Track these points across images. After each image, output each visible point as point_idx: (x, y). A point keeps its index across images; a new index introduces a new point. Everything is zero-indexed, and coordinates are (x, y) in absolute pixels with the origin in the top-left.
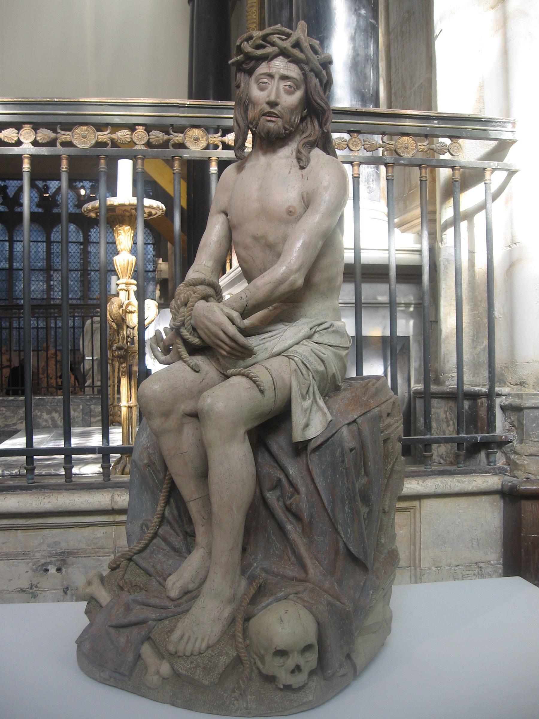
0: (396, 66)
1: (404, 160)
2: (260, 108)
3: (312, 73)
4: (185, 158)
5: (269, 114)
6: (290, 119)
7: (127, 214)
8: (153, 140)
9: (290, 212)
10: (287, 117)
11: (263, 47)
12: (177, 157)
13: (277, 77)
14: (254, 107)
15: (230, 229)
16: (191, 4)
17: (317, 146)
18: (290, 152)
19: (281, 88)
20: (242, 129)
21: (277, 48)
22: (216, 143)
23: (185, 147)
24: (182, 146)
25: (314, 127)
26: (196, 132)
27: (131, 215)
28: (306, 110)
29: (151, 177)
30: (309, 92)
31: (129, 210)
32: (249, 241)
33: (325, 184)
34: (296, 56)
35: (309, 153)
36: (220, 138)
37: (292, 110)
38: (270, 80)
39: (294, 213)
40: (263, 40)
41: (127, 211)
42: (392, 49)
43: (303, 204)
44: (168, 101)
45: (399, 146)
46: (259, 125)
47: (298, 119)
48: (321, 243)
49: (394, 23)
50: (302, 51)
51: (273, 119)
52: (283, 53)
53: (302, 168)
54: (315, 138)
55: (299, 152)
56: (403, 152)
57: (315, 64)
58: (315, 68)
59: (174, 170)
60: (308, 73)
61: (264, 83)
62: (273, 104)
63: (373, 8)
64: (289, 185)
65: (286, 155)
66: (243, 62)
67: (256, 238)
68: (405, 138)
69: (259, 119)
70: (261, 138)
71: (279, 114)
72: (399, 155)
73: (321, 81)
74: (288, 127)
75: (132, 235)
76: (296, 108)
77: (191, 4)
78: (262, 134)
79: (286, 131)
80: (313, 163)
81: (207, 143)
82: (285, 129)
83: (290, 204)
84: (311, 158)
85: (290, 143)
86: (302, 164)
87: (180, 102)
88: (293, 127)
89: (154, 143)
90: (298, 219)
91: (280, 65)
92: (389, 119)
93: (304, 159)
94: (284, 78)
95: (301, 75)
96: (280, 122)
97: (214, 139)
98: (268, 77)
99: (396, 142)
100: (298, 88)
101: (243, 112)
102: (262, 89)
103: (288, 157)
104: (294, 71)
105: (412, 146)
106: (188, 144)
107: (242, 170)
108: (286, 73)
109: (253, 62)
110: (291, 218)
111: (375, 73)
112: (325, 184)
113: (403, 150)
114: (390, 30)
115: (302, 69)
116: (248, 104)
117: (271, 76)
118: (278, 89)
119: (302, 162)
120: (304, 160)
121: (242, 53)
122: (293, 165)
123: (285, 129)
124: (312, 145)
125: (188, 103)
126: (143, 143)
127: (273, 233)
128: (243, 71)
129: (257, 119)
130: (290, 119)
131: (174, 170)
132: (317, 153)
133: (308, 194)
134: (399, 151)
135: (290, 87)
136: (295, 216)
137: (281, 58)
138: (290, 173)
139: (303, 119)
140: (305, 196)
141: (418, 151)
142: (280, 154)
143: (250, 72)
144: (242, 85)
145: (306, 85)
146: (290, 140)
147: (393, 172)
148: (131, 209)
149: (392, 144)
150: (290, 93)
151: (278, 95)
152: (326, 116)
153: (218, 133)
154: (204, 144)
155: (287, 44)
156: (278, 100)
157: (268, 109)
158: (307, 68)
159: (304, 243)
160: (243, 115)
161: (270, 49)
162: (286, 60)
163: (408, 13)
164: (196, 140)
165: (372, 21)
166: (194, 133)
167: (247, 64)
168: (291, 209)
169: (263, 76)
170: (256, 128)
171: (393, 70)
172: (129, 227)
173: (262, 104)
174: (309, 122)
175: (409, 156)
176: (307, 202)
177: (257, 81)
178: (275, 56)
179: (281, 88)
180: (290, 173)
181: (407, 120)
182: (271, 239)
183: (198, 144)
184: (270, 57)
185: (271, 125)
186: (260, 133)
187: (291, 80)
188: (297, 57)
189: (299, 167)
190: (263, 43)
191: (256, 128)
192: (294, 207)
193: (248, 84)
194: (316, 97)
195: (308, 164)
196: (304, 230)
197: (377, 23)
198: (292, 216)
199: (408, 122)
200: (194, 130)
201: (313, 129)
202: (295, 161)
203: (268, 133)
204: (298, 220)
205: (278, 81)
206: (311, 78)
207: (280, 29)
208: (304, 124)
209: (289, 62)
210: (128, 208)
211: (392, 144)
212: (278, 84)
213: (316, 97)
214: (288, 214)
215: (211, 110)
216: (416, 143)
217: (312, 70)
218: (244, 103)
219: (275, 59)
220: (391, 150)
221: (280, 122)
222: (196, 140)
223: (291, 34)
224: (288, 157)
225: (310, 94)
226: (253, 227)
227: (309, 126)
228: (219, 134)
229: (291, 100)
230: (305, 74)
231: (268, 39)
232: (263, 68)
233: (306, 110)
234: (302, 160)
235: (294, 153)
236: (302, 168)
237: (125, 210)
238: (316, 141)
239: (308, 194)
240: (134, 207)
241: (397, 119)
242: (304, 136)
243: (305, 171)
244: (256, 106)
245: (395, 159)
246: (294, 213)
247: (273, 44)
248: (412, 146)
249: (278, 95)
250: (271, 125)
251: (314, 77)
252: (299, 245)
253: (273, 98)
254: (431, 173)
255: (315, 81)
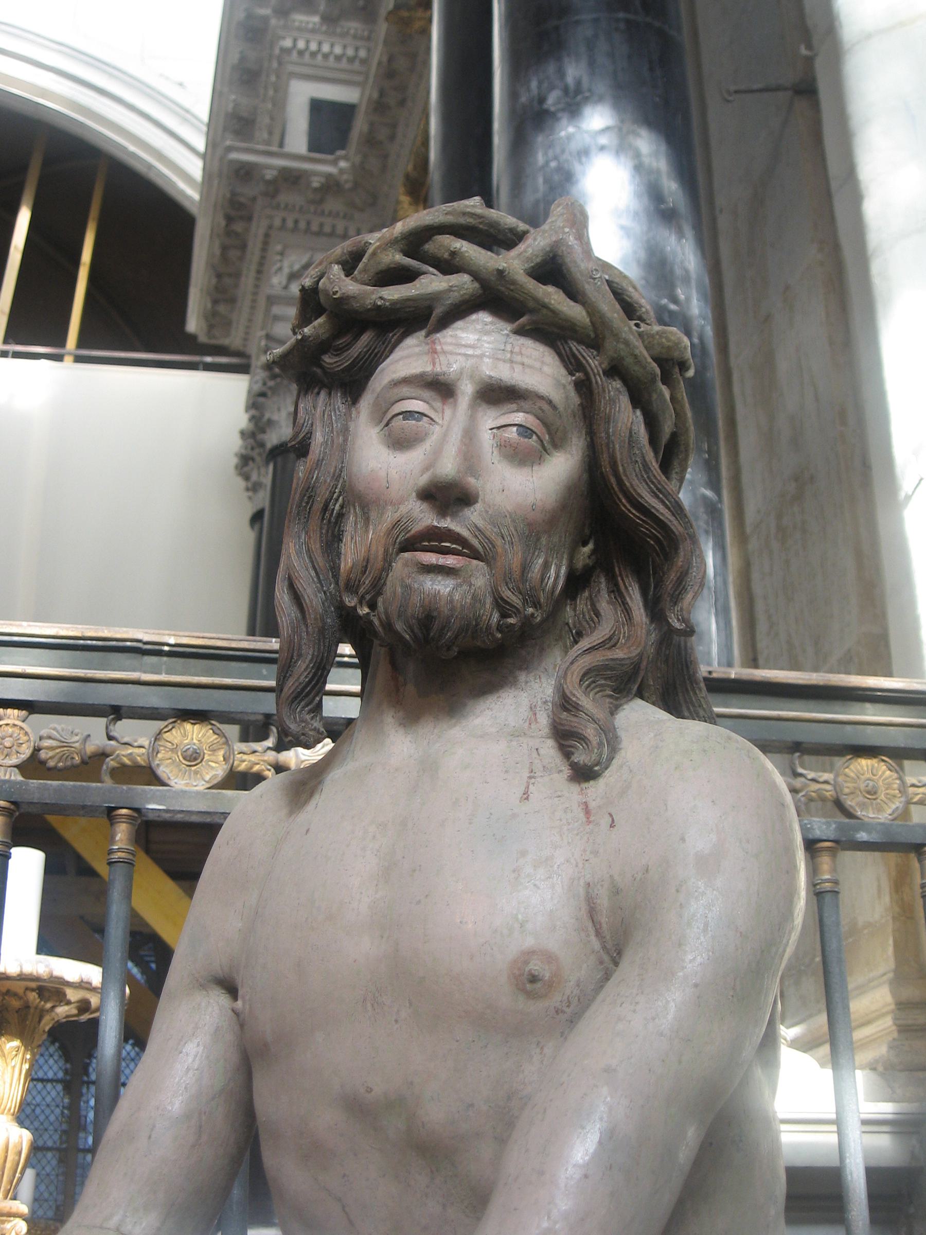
0: (770, 617)
1: (869, 832)
2: (390, 517)
3: (617, 384)
4: (151, 816)
5: (432, 539)
6: (525, 568)
7: (16, 1004)
8: (51, 754)
9: (530, 982)
10: (513, 557)
11: (404, 276)
12: (124, 811)
13: (467, 390)
14: (367, 520)
15: (250, 1058)
16: (257, 527)
17: (640, 695)
18: (524, 712)
19: (486, 438)
20: (310, 618)
21: (465, 278)
22: (256, 768)
23: (156, 780)
24: (148, 775)
25: (627, 611)
26: (194, 734)
27: (27, 1007)
28: (591, 546)
29: (147, 925)
30: (605, 459)
31: (21, 992)
32: (327, 1120)
33: (699, 842)
34: (545, 306)
35: (612, 713)
36: (271, 756)
37: (533, 530)
38: (438, 404)
39: (551, 985)
40: (407, 254)
41: (15, 995)
42: (755, 576)
43: (596, 944)
44: (106, 633)
45: (847, 787)
46: (388, 590)
47: (556, 576)
48: (692, 1135)
49: (759, 512)
50: (573, 294)
51: (450, 561)
52: (495, 298)
53: (583, 774)
54: (635, 652)
55: (565, 704)
56: (863, 806)
57: (627, 343)
58: (629, 361)
59: (111, 852)
60: (599, 380)
61: (408, 415)
62: (447, 496)
63: (707, 462)
64: (523, 853)
65: (503, 728)
66: (324, 346)
67: (361, 1109)
68: (864, 764)
69: (387, 566)
70: (397, 651)
71: (475, 542)
72: (849, 814)
73: (652, 423)
74: (515, 600)
75: (26, 1066)
76: (552, 520)
77: (257, 527)
78: (399, 626)
79: (504, 615)
80: (631, 750)
81: (226, 767)
82: (501, 605)
83: (529, 942)
84: (621, 733)
85: (522, 677)
86: (581, 757)
87: (146, 638)
88: (536, 605)
89: (51, 764)
90: (571, 1016)
91: (478, 347)
92: (812, 704)
93: (590, 732)
94: (496, 394)
95: (573, 393)
96: (480, 576)
97: (253, 758)
98: (427, 394)
99: (837, 776)
100: (555, 440)
101: (316, 546)
102: (400, 443)
103: (516, 734)
104: (537, 369)
105: (889, 786)
106: (163, 771)
107: (311, 795)
108: (506, 374)
109: (366, 338)
110: (535, 1007)
111: (722, 624)
112: (699, 842)
113: (861, 799)
114: (748, 530)
115: (572, 364)
116: (341, 515)
117: (441, 388)
118: (470, 435)
119: (580, 753)
120: (594, 740)
121: (319, 311)
122: (538, 766)
123: (501, 605)
124: (624, 683)
125: (172, 641)
126: (14, 760)
127: (444, 1082)
128: (323, 386)
129: (379, 564)
130: (525, 568)
131: (111, 852)
132: (640, 718)
133: (616, 891)
134: (849, 802)
135: (524, 430)
136: (556, 1000)
137: (483, 318)
138: (526, 796)
139: (577, 582)
140: (604, 902)
141: (909, 803)
142: (478, 721)
143: (352, 384)
144: (319, 437)
145: (591, 433)
146: (525, 665)
147: (834, 870)
148: (27, 989)
149: (826, 782)
150: (520, 457)
151: (470, 457)
152: (680, 561)
153: (265, 737)
154: (216, 769)
155: (514, 262)
156: (472, 480)
157: (425, 517)
158: (594, 363)
159: (609, 1138)
160: (320, 561)
161: (432, 283)
162: (506, 328)
163: (796, 480)
164: (193, 758)
165: (709, 493)
166: (185, 735)
167: (340, 351)
168: (535, 966)
169: (405, 390)
170: (373, 606)
171: (762, 626)
172: (16, 1043)
173: (401, 501)
174: (604, 594)
175: (884, 817)
176: (616, 930)
177: (384, 417)
178: (461, 310)
179: (486, 438)
180: (526, 796)
181: (868, 705)
182: (436, 1113)
183: (196, 773)
184: (438, 311)
185: (442, 587)
186: (388, 626)
187: (526, 405)
188: (554, 312)
189: (567, 771)
190: (408, 261)
191: (373, 606)
192: (549, 958)
193: (345, 431)
194: (636, 482)
195: (610, 759)
196: (608, 1070)
197: (720, 500)
198: (542, 1002)
199: (871, 714)
200: (188, 726)
201: (618, 623)
202: (549, 749)
203: (428, 618)
204: (573, 1021)
205: (473, 406)
206: (612, 401)
207: (479, 211)
208: (582, 603)
209: (520, 332)
210: (19, 987)
211: (826, 782)
212: (472, 418)
213: (636, 482)
214: (524, 991)
215: (245, 665)
216: (900, 778)
217: (615, 370)
218: (325, 508)
219: (459, 324)
220: (823, 799)
221: (480, 576)
222: (193, 758)
223: (525, 233)
224: (516, 734)
225: (607, 469)
226: (352, 1054)
227: (604, 605)
228: (270, 743)
229: (526, 485)
230: (584, 387)
231: (429, 247)
232: (408, 358)
233: (591, 546)
234: (582, 738)
235: (544, 720)
236: (583, 774)
237: (8, 992)
238: (636, 667)
239: (616, 891)
240: (33, 985)
241: (837, 705)
242: (585, 644)
243: (596, 790)
244: (373, 515)
245: (841, 828)
246: (551, 985)
247: (448, 265)
248: (889, 786)
249: (470, 457)
250: (442, 587)
251: (624, 401)
252: (582, 1149)
253: (448, 467)
254: (897, 891)
255: (626, 418)
